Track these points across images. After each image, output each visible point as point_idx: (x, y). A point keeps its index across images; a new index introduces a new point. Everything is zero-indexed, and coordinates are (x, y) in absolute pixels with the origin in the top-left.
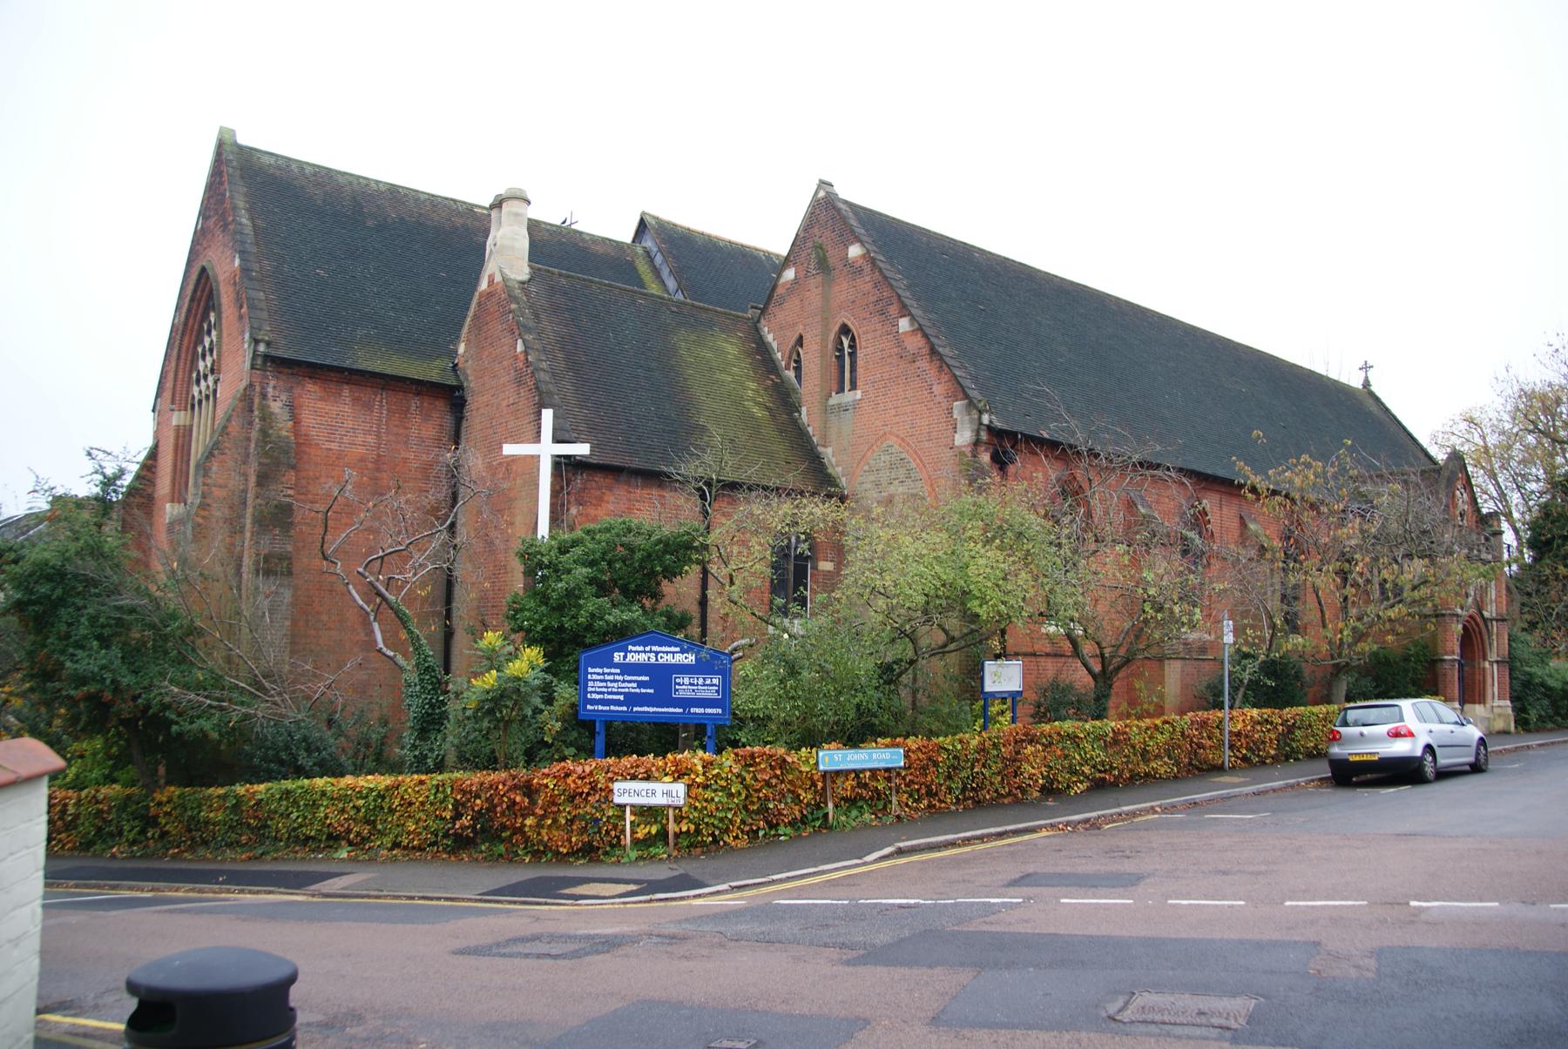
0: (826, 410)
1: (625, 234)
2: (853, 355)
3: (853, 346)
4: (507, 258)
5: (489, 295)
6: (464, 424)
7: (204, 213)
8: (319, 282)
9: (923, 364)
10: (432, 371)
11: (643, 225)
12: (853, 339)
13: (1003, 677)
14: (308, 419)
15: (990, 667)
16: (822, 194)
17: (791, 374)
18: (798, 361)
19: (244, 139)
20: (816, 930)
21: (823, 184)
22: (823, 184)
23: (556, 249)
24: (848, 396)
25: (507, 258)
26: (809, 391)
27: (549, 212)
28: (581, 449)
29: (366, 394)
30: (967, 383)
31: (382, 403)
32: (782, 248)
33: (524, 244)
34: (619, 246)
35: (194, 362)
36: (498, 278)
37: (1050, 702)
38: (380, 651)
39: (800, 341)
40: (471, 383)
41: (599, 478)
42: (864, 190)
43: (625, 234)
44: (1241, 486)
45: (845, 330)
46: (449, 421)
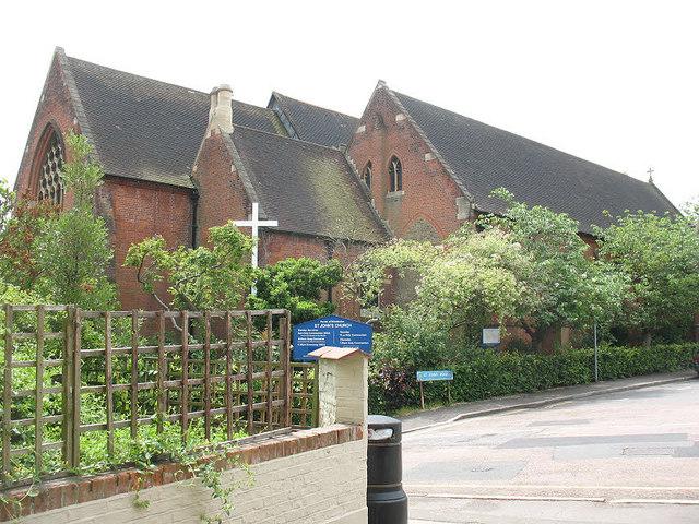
0: (385, 200)
1: (264, 104)
2: (399, 172)
3: (399, 167)
4: (222, 121)
5: (212, 141)
6: (198, 208)
7: (47, 92)
8: (115, 129)
9: (439, 178)
10: (183, 181)
11: (273, 99)
12: (399, 163)
13: (491, 336)
14: (120, 207)
15: (486, 332)
16: (380, 87)
17: (364, 181)
18: (368, 174)
19: (70, 53)
20: (630, 445)
21: (380, 81)
22: (380, 81)
23: (241, 112)
24: (397, 194)
25: (222, 121)
26: (377, 187)
27: (238, 96)
28: (273, 223)
29: (148, 193)
30: (277, 127)
31: (155, 196)
32: (359, 117)
33: (230, 114)
34: (262, 109)
35: (41, 175)
36: (217, 132)
37: (510, 345)
38: (175, 328)
39: (370, 164)
40: (203, 189)
41: (278, 238)
42: (401, 85)
43: (264, 104)
44: (596, 237)
45: (394, 159)
46: (189, 207)
